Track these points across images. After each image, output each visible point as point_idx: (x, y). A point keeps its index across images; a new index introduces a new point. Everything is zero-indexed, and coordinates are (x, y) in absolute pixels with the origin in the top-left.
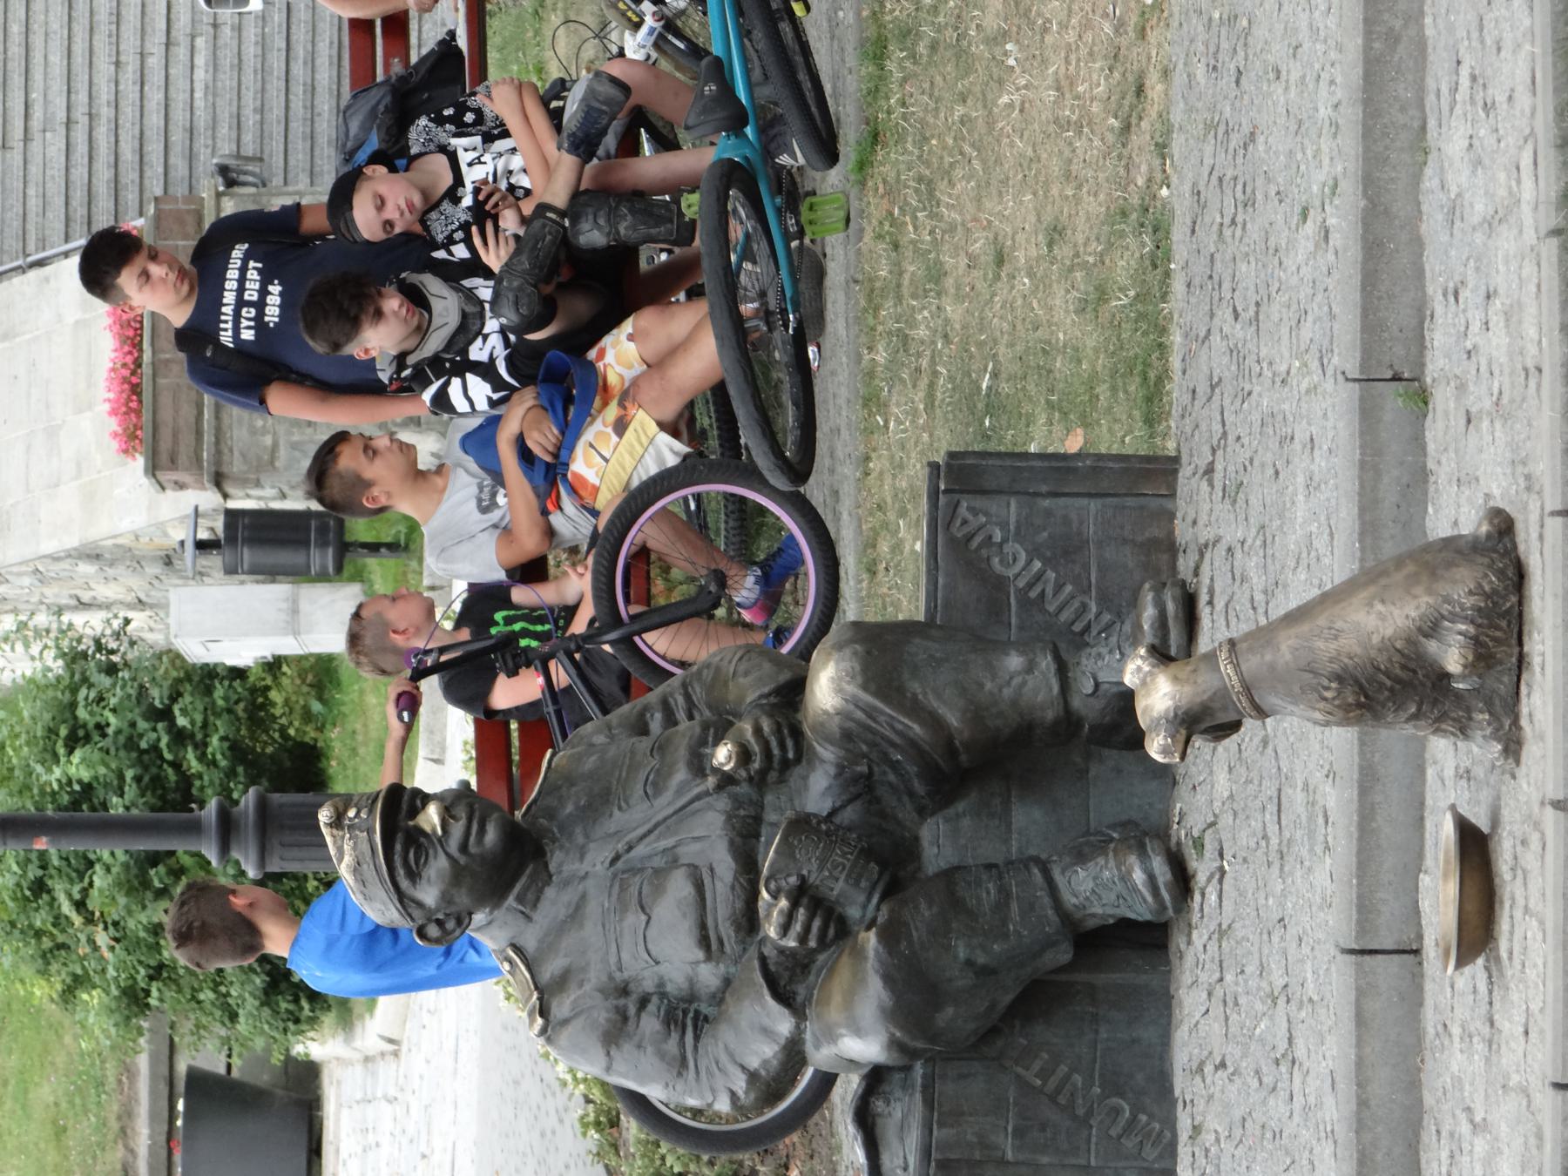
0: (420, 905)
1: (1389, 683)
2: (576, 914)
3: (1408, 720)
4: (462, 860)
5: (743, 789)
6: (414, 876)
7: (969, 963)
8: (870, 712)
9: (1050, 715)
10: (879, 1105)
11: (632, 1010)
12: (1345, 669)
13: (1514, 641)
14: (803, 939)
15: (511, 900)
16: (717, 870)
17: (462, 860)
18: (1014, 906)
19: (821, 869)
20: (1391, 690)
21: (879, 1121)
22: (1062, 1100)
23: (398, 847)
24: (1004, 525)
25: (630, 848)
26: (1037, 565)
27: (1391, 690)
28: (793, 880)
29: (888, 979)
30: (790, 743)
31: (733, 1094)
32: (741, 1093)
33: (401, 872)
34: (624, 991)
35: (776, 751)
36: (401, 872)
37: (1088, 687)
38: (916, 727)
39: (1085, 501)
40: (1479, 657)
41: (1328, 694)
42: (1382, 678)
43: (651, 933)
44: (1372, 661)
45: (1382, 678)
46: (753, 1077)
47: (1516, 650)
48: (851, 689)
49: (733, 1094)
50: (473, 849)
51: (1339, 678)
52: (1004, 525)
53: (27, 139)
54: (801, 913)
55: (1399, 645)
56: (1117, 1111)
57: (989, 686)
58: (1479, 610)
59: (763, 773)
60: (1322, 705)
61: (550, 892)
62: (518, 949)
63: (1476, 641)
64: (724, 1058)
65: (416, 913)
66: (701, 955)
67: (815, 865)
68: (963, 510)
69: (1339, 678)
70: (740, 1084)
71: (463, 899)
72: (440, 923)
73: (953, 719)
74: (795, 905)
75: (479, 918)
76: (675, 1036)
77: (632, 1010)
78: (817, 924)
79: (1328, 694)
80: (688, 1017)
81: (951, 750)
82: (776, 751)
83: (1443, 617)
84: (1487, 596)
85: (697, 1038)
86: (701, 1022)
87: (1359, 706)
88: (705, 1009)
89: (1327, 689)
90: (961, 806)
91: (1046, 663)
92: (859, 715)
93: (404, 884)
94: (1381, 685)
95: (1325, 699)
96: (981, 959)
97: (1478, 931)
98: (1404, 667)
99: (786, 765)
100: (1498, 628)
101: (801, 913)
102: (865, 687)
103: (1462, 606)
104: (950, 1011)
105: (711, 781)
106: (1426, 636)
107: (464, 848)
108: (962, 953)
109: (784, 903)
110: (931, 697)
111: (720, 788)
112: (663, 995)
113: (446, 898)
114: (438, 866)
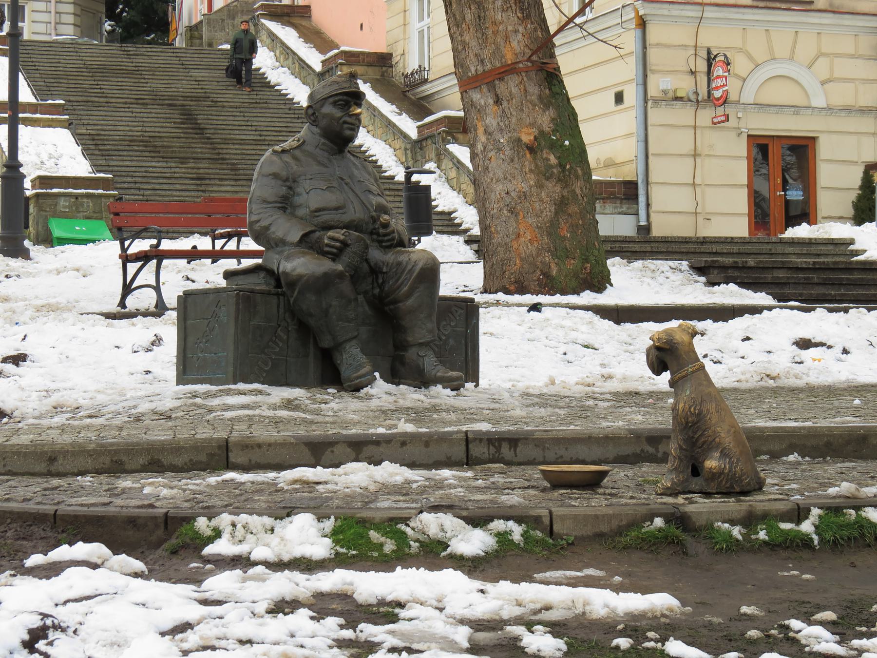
0: (322, 106)
1: (696, 436)
2: (320, 163)
3: (679, 445)
4: (341, 121)
5: (371, 227)
6: (335, 104)
7: (331, 306)
8: (411, 271)
9: (410, 339)
10: (262, 274)
11: (288, 184)
12: (704, 416)
13: (718, 490)
14: (327, 245)
15: (323, 140)
16: (344, 215)
17: (341, 121)
18: (347, 324)
19: (353, 252)
20: (693, 437)
21: (256, 275)
22: (271, 343)
23: (345, 97)
24: (456, 326)
25: (346, 184)
26: (444, 338)
27: (693, 437)
28: (349, 242)
29: (326, 275)
30: (388, 244)
31: (258, 221)
32: (258, 224)
33: (336, 98)
34: (294, 181)
35: (386, 238)
36: (336, 98)
37: (421, 354)
38: (406, 288)
39: (464, 355)
40: (714, 474)
41: (692, 409)
42: (699, 433)
43: (319, 191)
44: (710, 428)
45: (699, 433)
46: (267, 228)
47: (714, 491)
48: (420, 265)
49: (258, 221)
50: (346, 126)
51: (700, 414)
52: (456, 326)
53: (102, 155)
54: (338, 244)
55: (717, 439)
56: (267, 365)
57: (422, 316)
58: (735, 474)
59: (378, 234)
60: (687, 406)
61: (326, 155)
62: (304, 142)
63: (721, 473)
64: (274, 217)
65: (318, 105)
66: (312, 209)
67: (355, 250)
68: (460, 311)
69: (700, 414)
70: (264, 223)
71: (324, 123)
72: (314, 113)
73: (410, 302)
74: (342, 242)
75: (316, 130)
76: (279, 199)
77: (288, 184)
78: (335, 251)
79: (692, 409)
80: (285, 204)
81: (395, 302)
82: (386, 238)
83: (730, 459)
84: (740, 477)
85: (279, 208)
86: (284, 209)
87: (687, 423)
88: (288, 211)
89: (695, 408)
90: (367, 308)
91: (428, 338)
92: (409, 267)
93: (331, 100)
94: (696, 433)
95: (690, 408)
96: (331, 311)
97: (558, 482)
98: (704, 442)
99: (380, 242)
100: (727, 482)
101: (338, 244)
102: (422, 269)
103: (736, 467)
104: (314, 298)
105: (374, 214)
106: (721, 452)
107: (345, 122)
108: (334, 303)
109: (342, 237)
110: (418, 294)
111: (372, 217)
112: (293, 196)
113: (325, 116)
114: (337, 113)
